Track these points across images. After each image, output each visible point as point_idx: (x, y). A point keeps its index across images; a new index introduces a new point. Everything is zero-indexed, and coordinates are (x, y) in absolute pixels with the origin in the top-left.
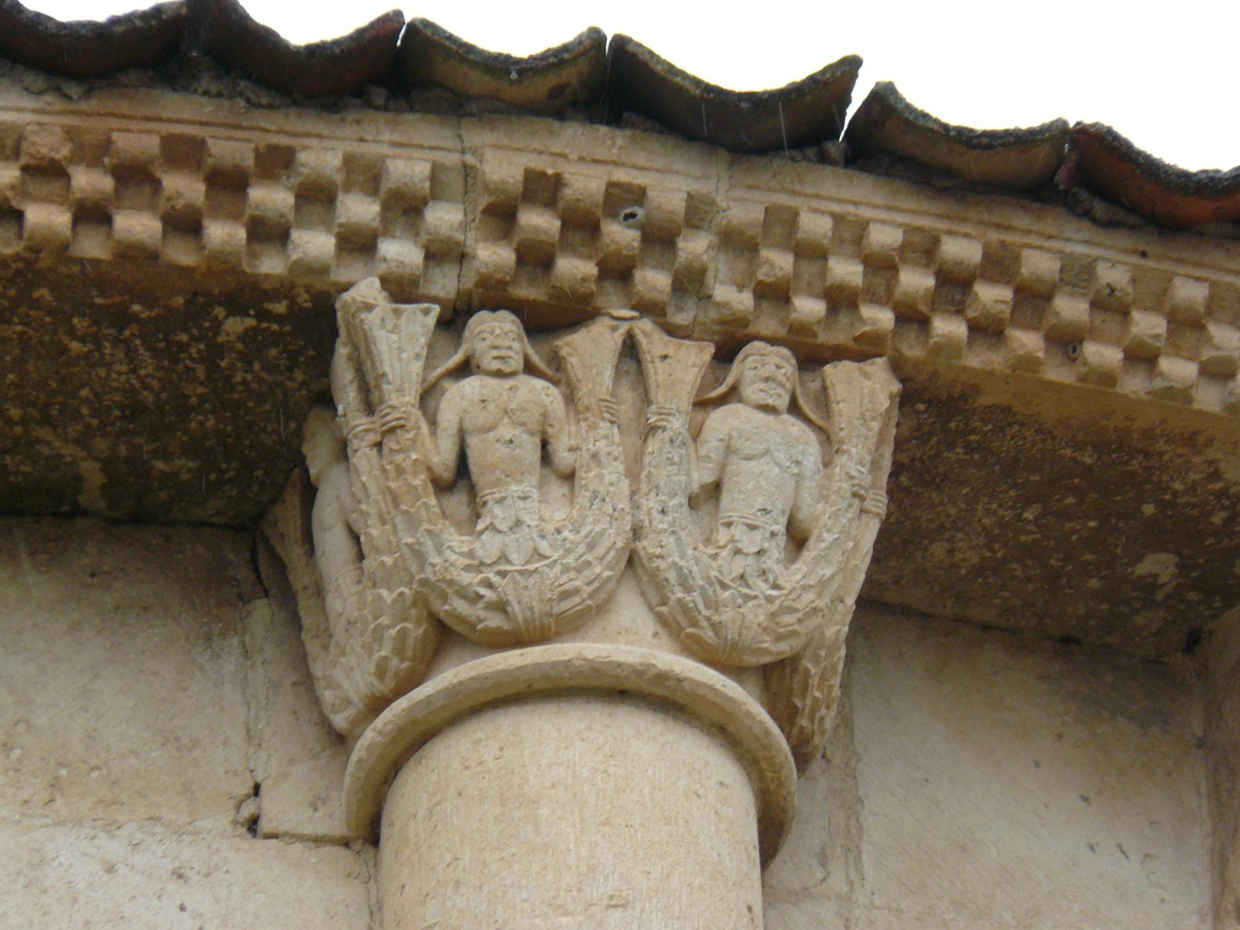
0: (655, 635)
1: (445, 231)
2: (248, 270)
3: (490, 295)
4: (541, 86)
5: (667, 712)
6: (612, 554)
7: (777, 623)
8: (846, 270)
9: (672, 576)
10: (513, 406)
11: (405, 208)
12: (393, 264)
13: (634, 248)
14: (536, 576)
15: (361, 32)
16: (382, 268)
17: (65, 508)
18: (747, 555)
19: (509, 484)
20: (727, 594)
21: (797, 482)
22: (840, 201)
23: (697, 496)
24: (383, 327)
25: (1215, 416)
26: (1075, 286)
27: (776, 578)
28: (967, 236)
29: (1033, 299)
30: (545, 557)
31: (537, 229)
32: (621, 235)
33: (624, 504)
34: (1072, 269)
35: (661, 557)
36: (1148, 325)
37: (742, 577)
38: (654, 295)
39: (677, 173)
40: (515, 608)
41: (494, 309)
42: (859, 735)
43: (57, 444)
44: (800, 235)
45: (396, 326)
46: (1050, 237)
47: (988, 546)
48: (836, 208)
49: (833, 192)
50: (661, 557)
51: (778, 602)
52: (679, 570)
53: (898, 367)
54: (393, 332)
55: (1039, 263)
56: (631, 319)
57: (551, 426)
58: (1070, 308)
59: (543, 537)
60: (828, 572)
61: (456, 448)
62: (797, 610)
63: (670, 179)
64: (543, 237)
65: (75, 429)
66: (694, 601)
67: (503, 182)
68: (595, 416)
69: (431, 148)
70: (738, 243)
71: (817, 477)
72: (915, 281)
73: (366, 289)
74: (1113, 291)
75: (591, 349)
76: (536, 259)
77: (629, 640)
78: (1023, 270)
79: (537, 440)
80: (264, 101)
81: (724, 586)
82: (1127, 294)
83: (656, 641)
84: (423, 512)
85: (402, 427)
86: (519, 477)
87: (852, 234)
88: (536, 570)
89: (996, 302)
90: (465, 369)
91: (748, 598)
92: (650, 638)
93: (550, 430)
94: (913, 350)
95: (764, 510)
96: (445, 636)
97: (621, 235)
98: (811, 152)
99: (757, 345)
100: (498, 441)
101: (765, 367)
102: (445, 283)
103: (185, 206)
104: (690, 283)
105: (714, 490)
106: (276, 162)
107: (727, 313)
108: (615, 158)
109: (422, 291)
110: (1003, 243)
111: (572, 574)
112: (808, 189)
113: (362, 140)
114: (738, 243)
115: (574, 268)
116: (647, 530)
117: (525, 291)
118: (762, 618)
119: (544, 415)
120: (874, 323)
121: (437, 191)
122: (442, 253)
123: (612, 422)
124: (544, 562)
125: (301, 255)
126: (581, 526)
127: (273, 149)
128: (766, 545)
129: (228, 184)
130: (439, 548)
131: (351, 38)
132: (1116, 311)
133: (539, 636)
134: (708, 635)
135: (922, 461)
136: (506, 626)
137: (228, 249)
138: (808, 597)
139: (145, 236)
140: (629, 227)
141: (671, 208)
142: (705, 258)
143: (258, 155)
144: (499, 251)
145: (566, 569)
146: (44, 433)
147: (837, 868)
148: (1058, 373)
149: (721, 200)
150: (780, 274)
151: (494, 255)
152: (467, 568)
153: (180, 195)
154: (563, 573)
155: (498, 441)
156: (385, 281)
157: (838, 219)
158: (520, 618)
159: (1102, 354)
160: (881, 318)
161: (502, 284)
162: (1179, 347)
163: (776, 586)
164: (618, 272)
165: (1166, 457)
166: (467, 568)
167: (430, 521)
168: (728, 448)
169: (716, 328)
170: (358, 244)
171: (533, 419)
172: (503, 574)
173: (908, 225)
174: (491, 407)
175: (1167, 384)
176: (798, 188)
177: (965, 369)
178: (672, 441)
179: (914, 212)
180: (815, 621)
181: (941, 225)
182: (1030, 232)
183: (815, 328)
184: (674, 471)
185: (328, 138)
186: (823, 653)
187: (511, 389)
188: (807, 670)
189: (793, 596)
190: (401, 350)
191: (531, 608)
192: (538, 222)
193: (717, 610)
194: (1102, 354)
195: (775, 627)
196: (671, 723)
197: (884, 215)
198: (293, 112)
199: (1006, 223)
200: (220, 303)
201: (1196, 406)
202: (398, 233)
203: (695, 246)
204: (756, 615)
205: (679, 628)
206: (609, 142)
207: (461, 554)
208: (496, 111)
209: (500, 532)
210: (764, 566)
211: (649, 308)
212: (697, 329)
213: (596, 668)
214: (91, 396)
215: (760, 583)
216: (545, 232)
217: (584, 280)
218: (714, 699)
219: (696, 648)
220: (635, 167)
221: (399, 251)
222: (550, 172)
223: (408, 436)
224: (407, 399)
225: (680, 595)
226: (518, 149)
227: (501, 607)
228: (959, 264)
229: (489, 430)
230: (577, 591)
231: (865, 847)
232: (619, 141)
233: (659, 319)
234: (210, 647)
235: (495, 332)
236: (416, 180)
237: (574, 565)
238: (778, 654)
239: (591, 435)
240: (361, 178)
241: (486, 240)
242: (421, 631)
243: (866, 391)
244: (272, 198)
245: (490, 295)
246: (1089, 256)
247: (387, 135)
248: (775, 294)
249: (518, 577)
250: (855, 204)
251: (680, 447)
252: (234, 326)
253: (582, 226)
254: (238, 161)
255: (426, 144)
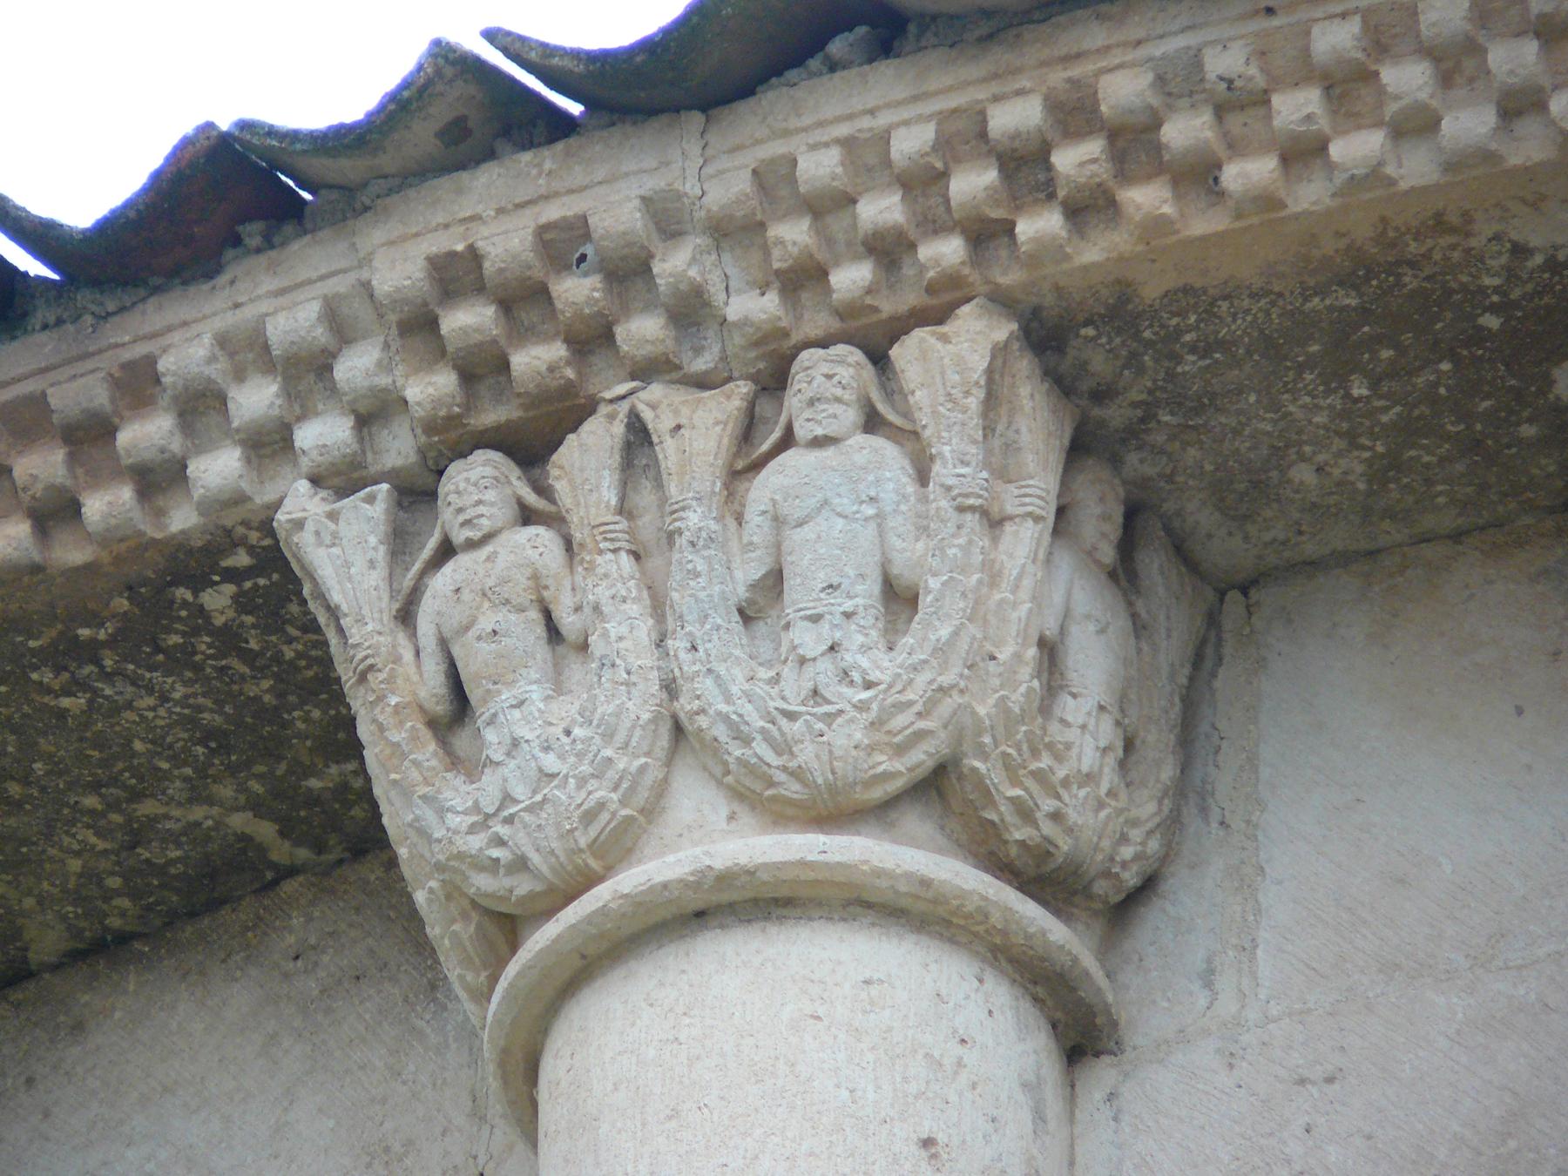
0: (732, 817)
1: (361, 382)
2: (159, 535)
3: (450, 441)
4: (422, 136)
5: (767, 917)
6: (638, 733)
7: (889, 732)
8: (881, 209)
9: (721, 732)
10: (490, 582)
11: (308, 373)
12: (314, 454)
13: (597, 301)
14: (548, 808)
15: (157, 176)
16: (305, 463)
17: (269, 875)
18: (814, 659)
19: (499, 692)
20: (798, 725)
21: (879, 525)
22: (850, 117)
23: (751, 602)
24: (320, 543)
25: (1437, 185)
26: (1191, 94)
27: (864, 672)
28: (1020, 93)
29: (1134, 144)
30: (553, 776)
31: (464, 330)
32: (577, 291)
33: (648, 659)
34: (1176, 75)
35: (702, 711)
36: (1296, 107)
37: (815, 692)
38: (648, 350)
39: (627, 174)
40: (535, 859)
41: (463, 455)
42: (1265, 772)
43: (176, 813)
44: (802, 190)
45: (335, 535)
46: (1139, 43)
47: (1354, 445)
48: (843, 130)
49: (828, 112)
50: (702, 711)
51: (875, 706)
52: (725, 718)
53: (1002, 301)
54: (334, 545)
55: (1123, 90)
56: (632, 393)
57: (546, 587)
58: (1185, 131)
59: (547, 749)
60: (944, 632)
61: (443, 667)
62: (910, 704)
63: (613, 188)
64: (478, 337)
65: (175, 788)
66: (756, 754)
67: (398, 290)
68: (590, 553)
69: (322, 278)
70: (730, 232)
71: (903, 508)
72: (972, 183)
73: (300, 502)
74: (1230, 82)
75: (586, 461)
76: (482, 369)
77: (705, 838)
78: (1103, 108)
79: (534, 614)
80: (111, 307)
81: (791, 716)
82: (1251, 78)
83: (734, 824)
84: (415, 774)
85: (371, 667)
86: (511, 677)
87: (871, 158)
88: (545, 800)
89: (1082, 164)
90: (447, 551)
91: (829, 718)
92: (724, 825)
93: (545, 594)
94: (1010, 277)
95: (831, 586)
96: (507, 926)
97: (577, 291)
98: (814, 63)
99: (806, 356)
100: (479, 638)
101: (829, 379)
102: (398, 447)
103: (46, 489)
104: (691, 311)
105: (774, 582)
106: (138, 385)
107: (751, 330)
108: (543, 191)
109: (373, 469)
110: (1069, 80)
111: (592, 784)
112: (807, 120)
113: (237, 306)
114: (730, 232)
115: (535, 359)
116: (680, 681)
117: (492, 415)
118: (858, 735)
119: (535, 577)
120: (937, 262)
121: (342, 331)
122: (371, 415)
123: (615, 551)
124: (556, 782)
125: (202, 491)
126: (593, 713)
127: (127, 366)
128: (838, 635)
129: (89, 436)
130: (442, 811)
131: (145, 190)
132: (1254, 104)
133: (590, 881)
134: (793, 789)
135: (1163, 389)
136: (539, 888)
137: (113, 521)
138: (922, 679)
139: (9, 550)
140: (586, 275)
141: (622, 228)
142: (693, 273)
143: (116, 384)
144: (434, 379)
145: (582, 781)
146: (148, 808)
147: (1226, 983)
148: (1204, 223)
149: (691, 187)
150: (795, 251)
151: (432, 388)
152: (472, 829)
153: (34, 477)
154: (579, 787)
155: (479, 638)
156: (316, 481)
157: (848, 144)
158: (545, 869)
159: (1248, 173)
160: (947, 251)
161: (452, 421)
162: (1357, 115)
163: (869, 685)
164: (592, 339)
165: (1437, 256)
166: (472, 829)
167: (427, 782)
168: (776, 518)
169: (752, 354)
170: (270, 444)
171: (520, 589)
172: (509, 820)
173: (940, 113)
174: (466, 595)
175: (1346, 176)
176: (794, 123)
177: (1085, 269)
178: (693, 544)
179: (949, 89)
180: (947, 706)
181: (981, 94)
182: (1108, 48)
183: (869, 300)
184: (709, 581)
185: (195, 321)
186: (987, 740)
187: (488, 559)
188: (974, 770)
189: (898, 687)
190: (348, 564)
191: (552, 852)
192: (468, 320)
193: (792, 753)
194: (1248, 173)
195: (886, 739)
196: (773, 929)
197: (905, 113)
198: (152, 302)
199: (1075, 50)
200: (175, 583)
201: (1403, 185)
202: (320, 407)
203: (675, 264)
204: (848, 736)
205: (759, 799)
206: (534, 172)
207: (465, 813)
208: (390, 192)
209: (498, 764)
210: (843, 665)
211: (647, 370)
212: (733, 365)
213: (638, 903)
214: (150, 746)
215: (846, 691)
216: (477, 330)
217: (551, 369)
218: (812, 875)
219: (790, 811)
220: (571, 191)
221: (326, 433)
222: (460, 247)
223: (381, 676)
224: (370, 627)
225: (738, 753)
226: (417, 235)
227: (520, 864)
228: (1016, 135)
229: (467, 628)
230: (601, 805)
231: (1264, 935)
232: (548, 165)
233: (675, 375)
234: (434, 1000)
235: (478, 485)
236: (303, 333)
237: (591, 770)
238: (910, 770)
239: (589, 581)
240: (250, 356)
241: (417, 371)
242: (472, 929)
243: (946, 361)
244: (146, 433)
245: (450, 441)
246: (1189, 48)
247: (269, 284)
248: (803, 279)
249: (527, 817)
250: (872, 112)
251: (706, 547)
252: (218, 600)
253: (523, 301)
254: (84, 405)
255: (314, 275)
